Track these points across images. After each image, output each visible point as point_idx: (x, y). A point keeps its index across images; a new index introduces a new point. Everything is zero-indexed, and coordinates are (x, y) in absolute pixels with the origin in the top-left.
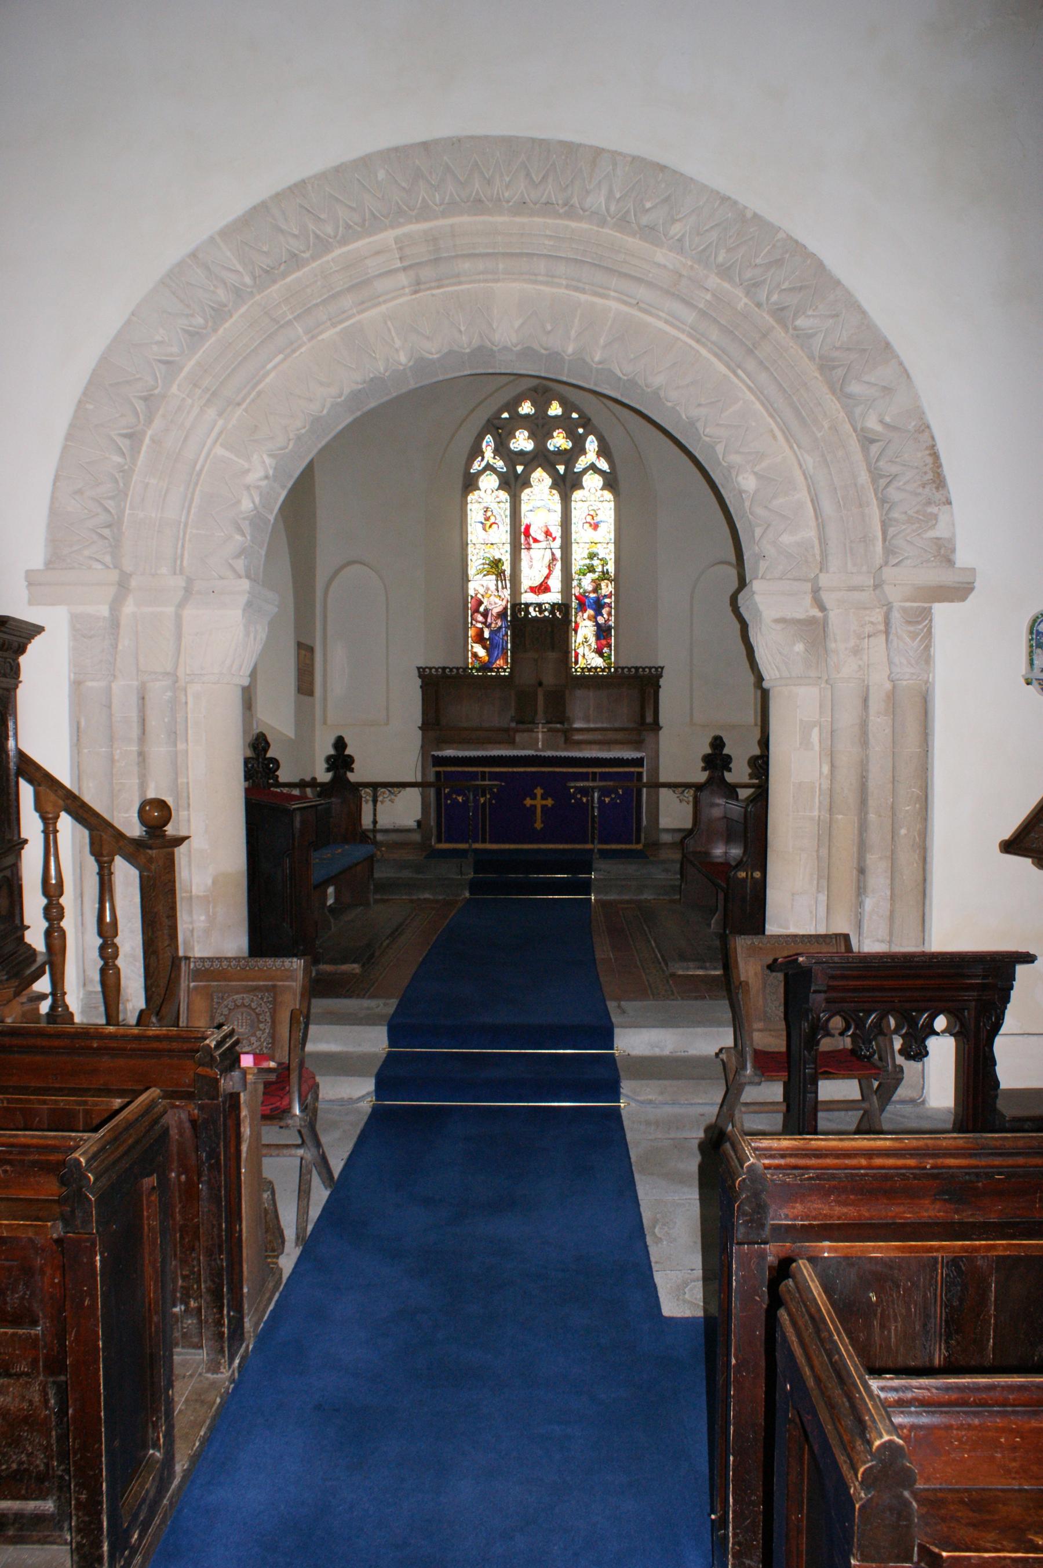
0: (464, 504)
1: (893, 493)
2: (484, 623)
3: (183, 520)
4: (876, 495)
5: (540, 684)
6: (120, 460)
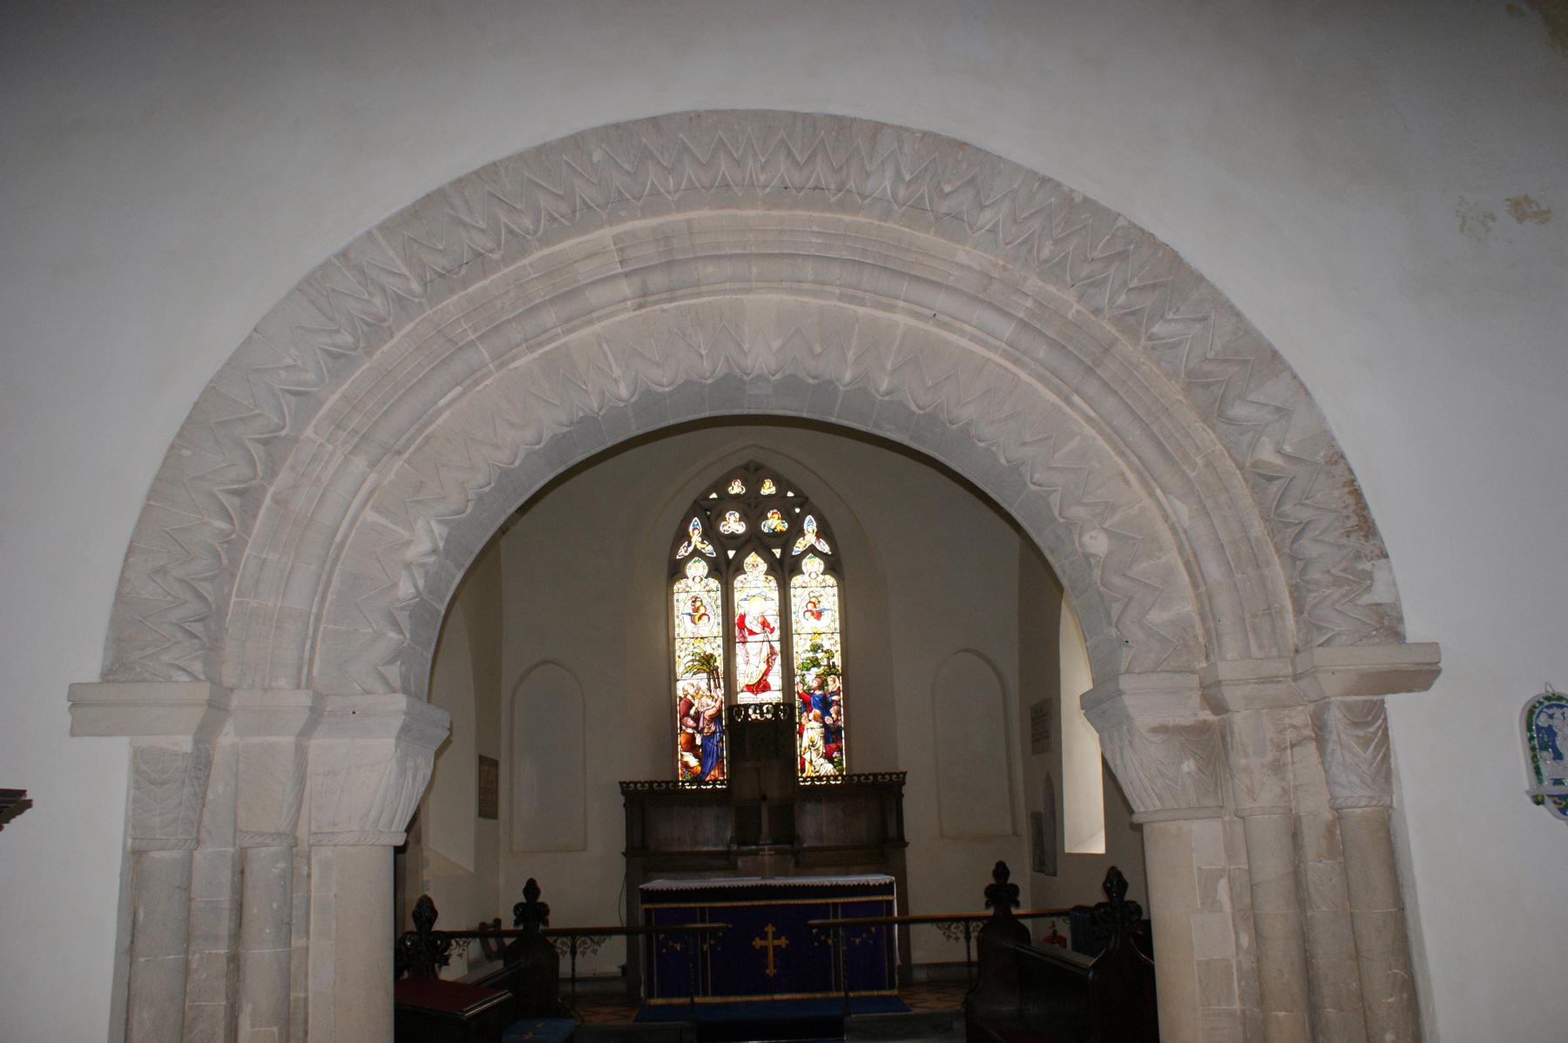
0: (669, 595)
1: (1308, 547)
2: (696, 728)
3: (314, 610)
4: (1278, 550)
5: (764, 798)
6: (223, 525)
